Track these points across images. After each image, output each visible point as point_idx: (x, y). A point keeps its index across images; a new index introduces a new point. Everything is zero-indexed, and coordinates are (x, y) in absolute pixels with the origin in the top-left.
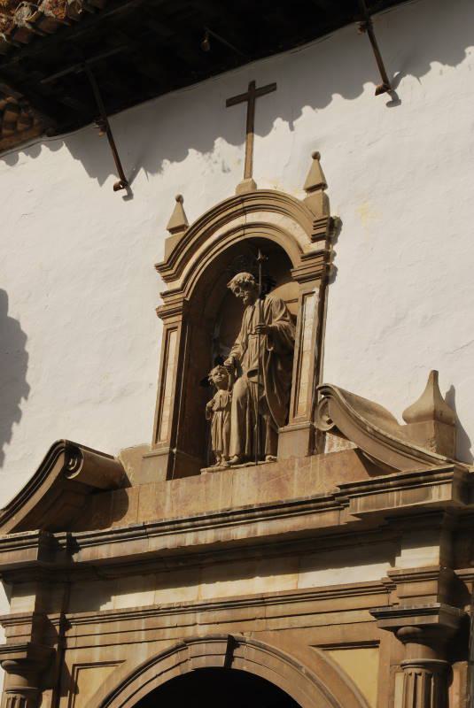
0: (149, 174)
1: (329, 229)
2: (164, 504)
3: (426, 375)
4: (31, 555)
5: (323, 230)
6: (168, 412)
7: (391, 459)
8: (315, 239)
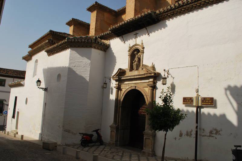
1: (144, 48)
3: (152, 63)
4: (117, 79)
6: (129, 65)
8: (142, 49)
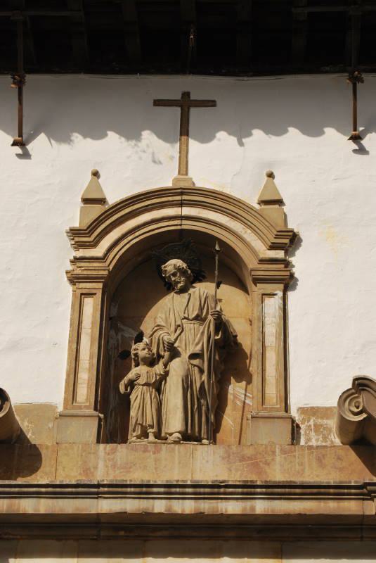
0: (53, 142)
1: (291, 241)
2: (96, 468)
8: (273, 247)
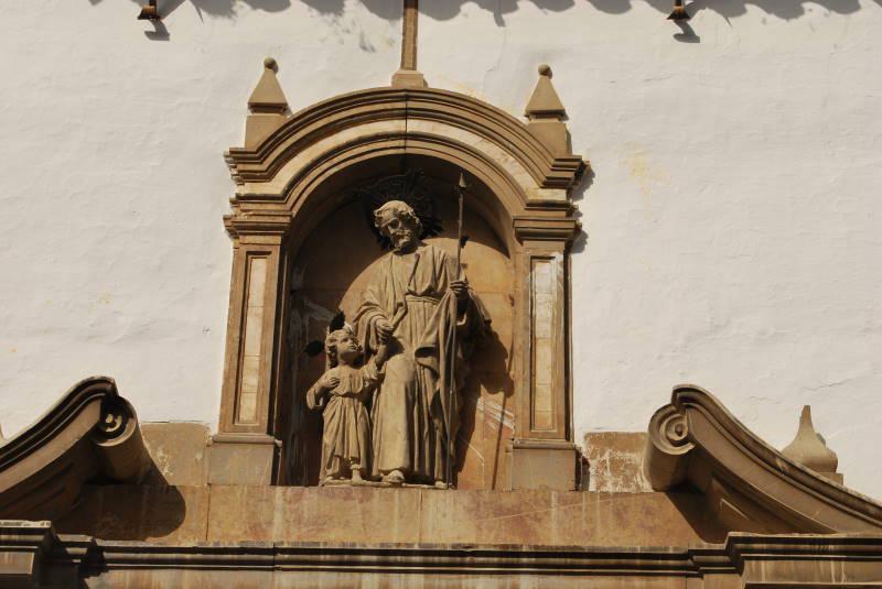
0: (203, 13)
1: (577, 175)
2: (270, 523)
5: (570, 175)
7: (817, 513)
8: (549, 184)
